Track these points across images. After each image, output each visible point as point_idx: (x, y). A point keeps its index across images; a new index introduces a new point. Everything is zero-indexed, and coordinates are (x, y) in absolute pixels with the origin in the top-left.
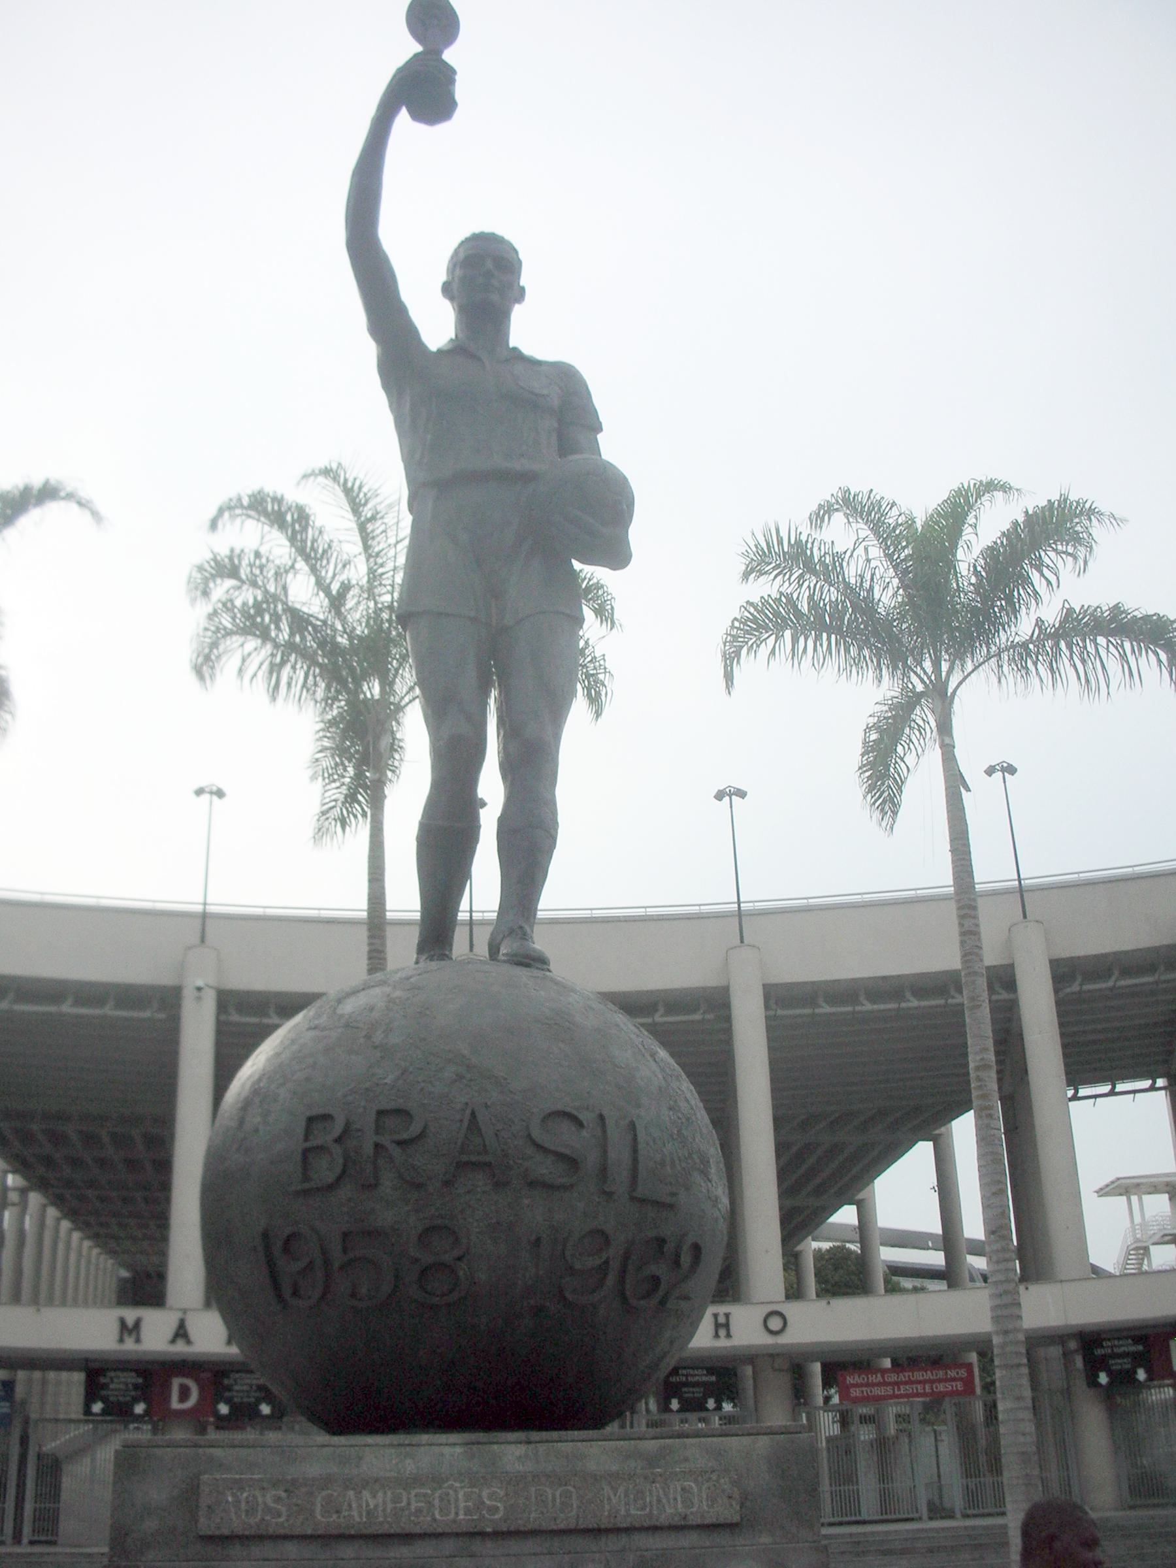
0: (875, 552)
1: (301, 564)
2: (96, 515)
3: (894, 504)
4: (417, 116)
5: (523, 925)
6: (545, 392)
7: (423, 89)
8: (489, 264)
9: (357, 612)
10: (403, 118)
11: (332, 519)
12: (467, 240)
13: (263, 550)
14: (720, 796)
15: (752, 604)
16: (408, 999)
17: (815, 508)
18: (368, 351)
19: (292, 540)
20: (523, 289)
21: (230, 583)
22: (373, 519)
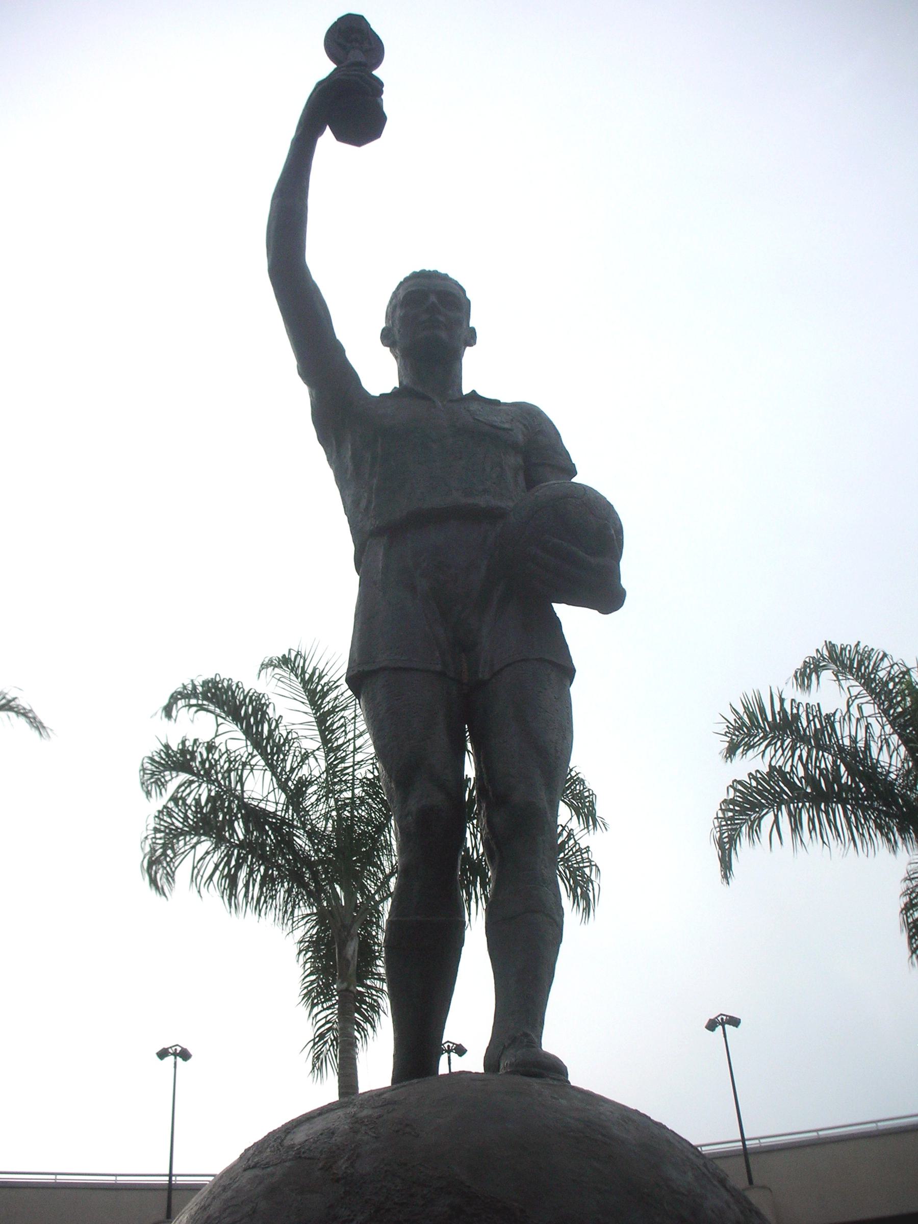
0: (870, 709)
1: (258, 760)
2: (36, 724)
3: (885, 655)
4: (341, 136)
5: (529, 1032)
6: (506, 426)
7: (348, 102)
8: (433, 299)
9: (319, 810)
10: (327, 141)
11: (291, 713)
12: (407, 280)
13: (217, 741)
14: (712, 1025)
15: (740, 782)
16: (380, 1116)
17: (800, 665)
18: (298, 397)
19: (247, 732)
20: (473, 331)
21: (184, 777)
22: (333, 711)
